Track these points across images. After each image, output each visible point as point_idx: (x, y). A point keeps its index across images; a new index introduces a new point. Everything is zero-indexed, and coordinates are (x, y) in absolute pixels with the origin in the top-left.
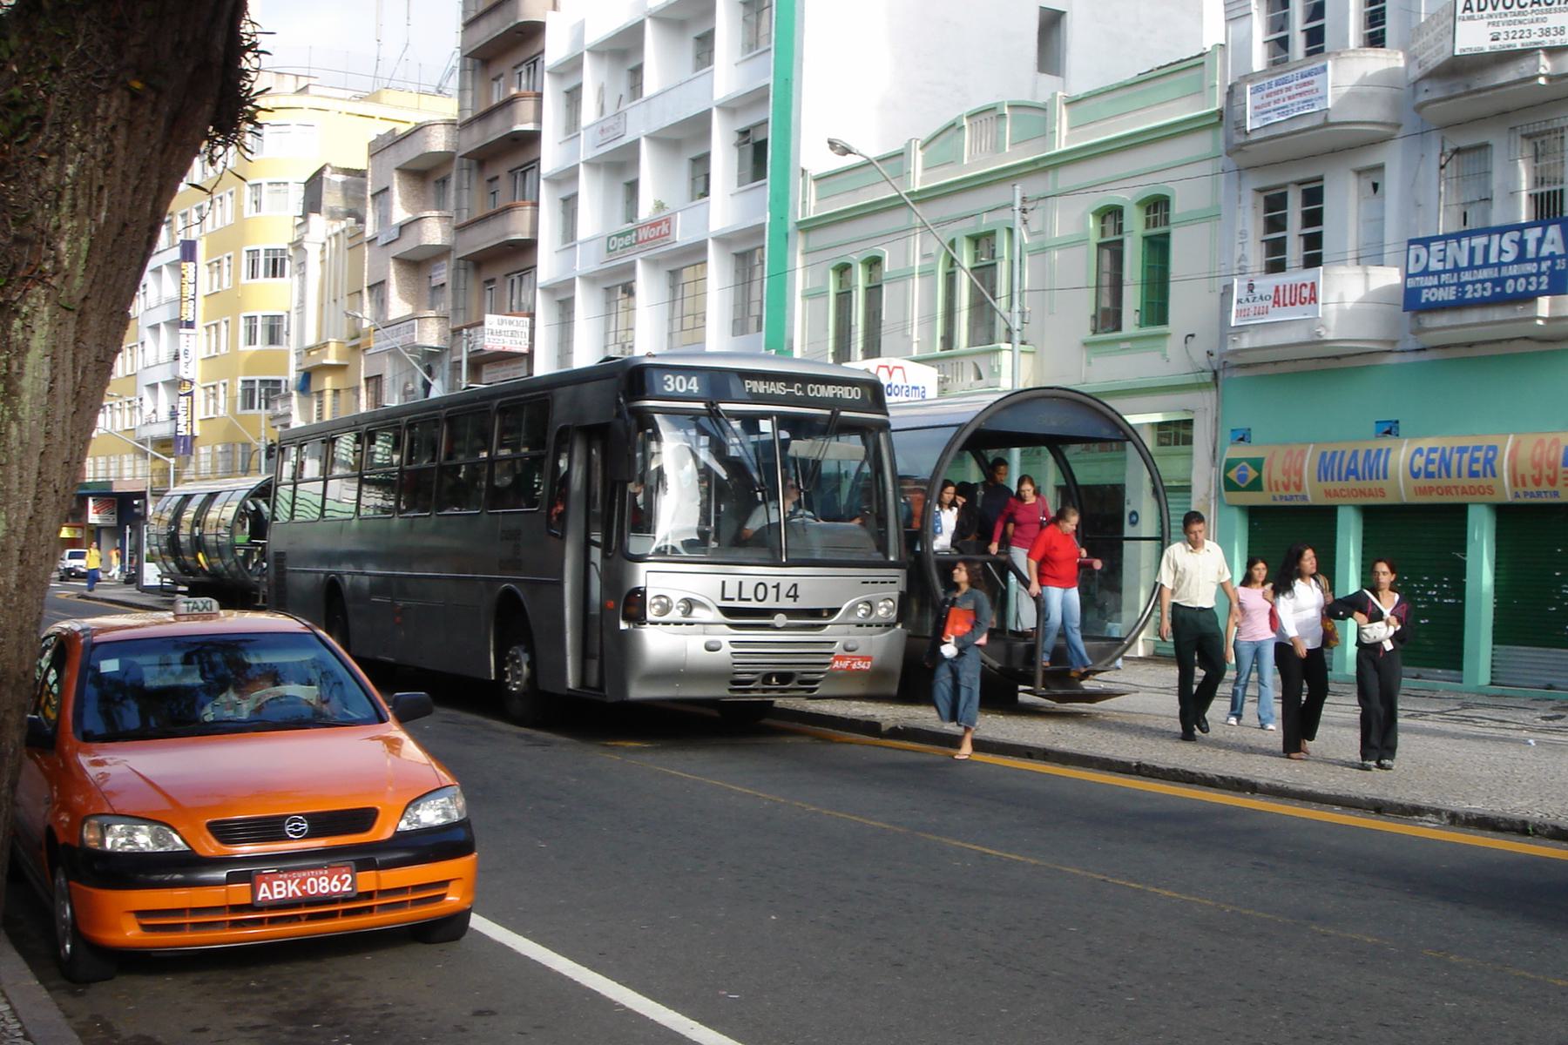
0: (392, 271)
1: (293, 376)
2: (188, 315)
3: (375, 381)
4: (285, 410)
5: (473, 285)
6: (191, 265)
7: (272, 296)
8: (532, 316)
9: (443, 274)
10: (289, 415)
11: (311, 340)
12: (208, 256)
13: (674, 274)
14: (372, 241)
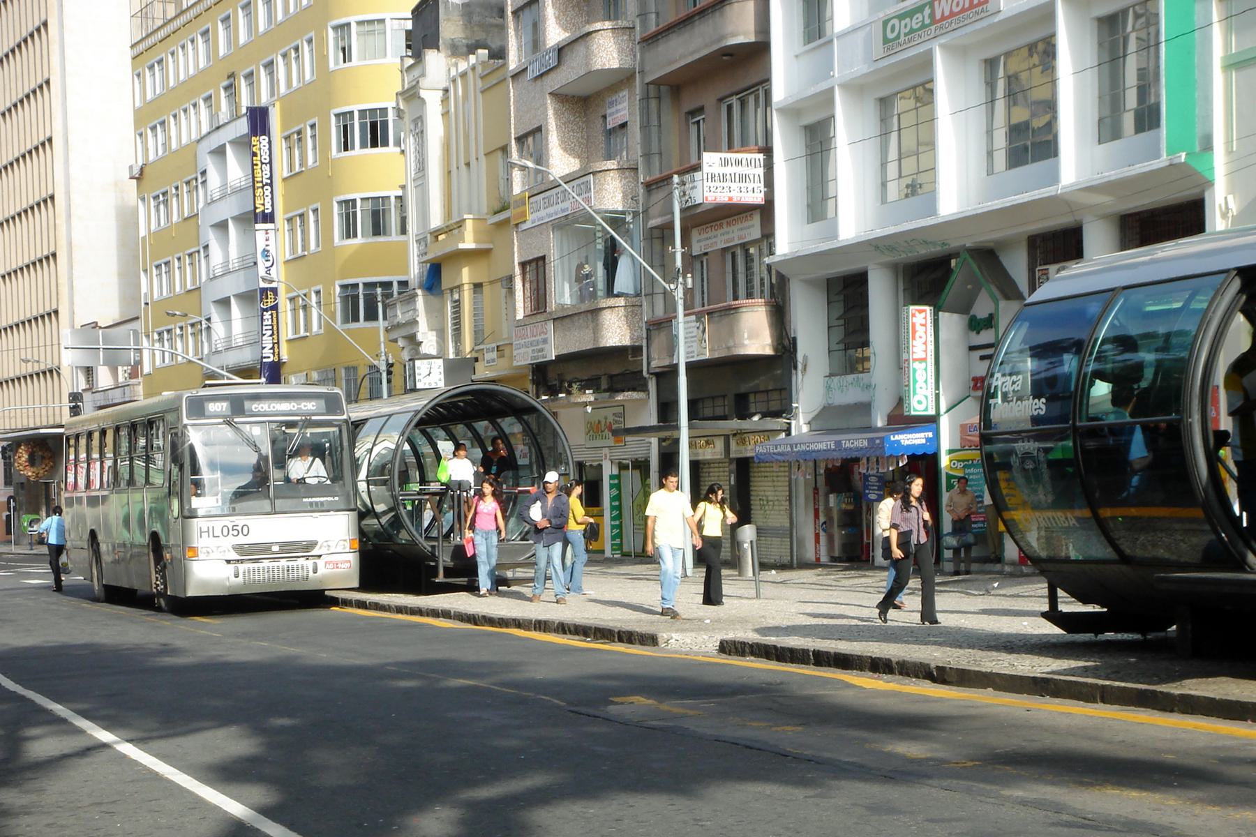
0: (551, 112)
1: (415, 271)
2: (263, 204)
3: (536, 267)
4: (409, 316)
5: (671, 120)
6: (264, 140)
7: (379, 172)
8: (768, 151)
9: (623, 109)
10: (414, 322)
11: (436, 221)
12: (285, 126)
13: (885, 103)
14: (516, 76)
